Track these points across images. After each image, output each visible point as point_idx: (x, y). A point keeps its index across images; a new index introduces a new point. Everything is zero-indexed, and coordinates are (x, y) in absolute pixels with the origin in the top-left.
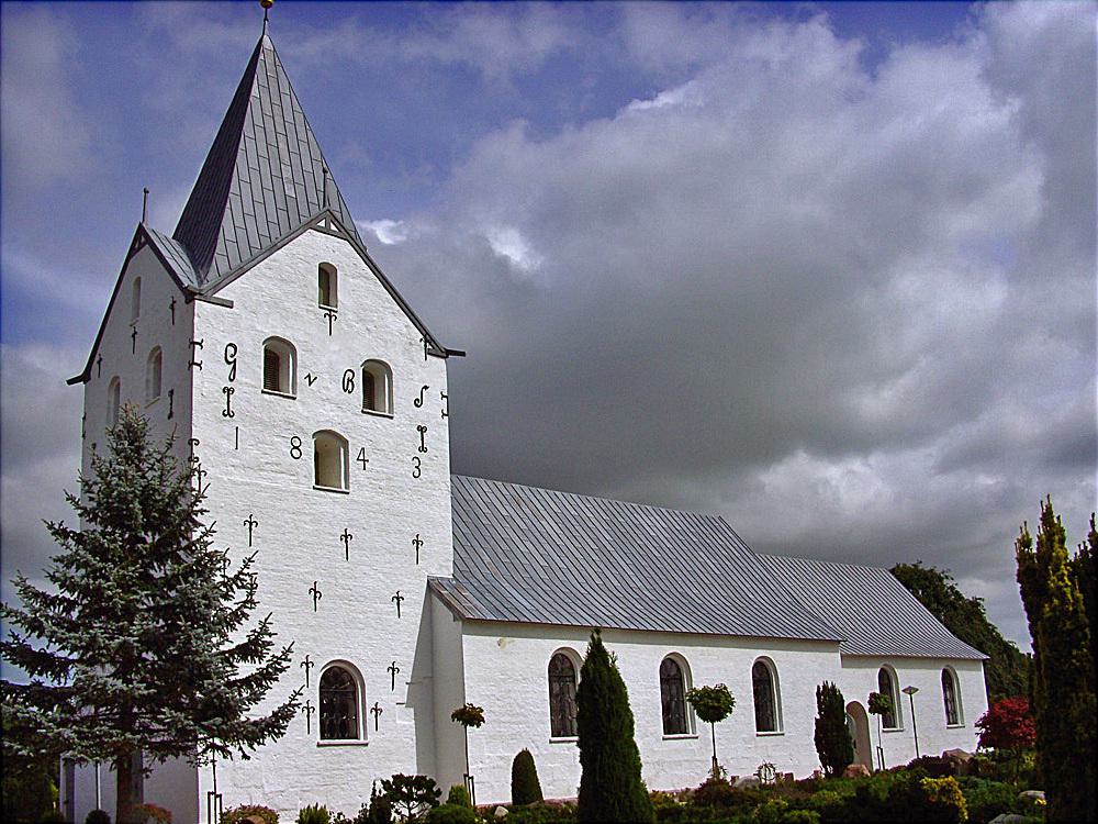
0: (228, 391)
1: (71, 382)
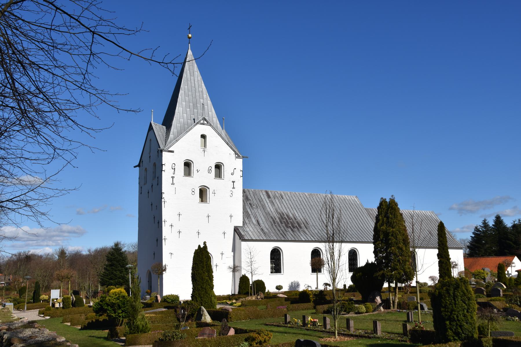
0: (173, 177)
1: (135, 167)
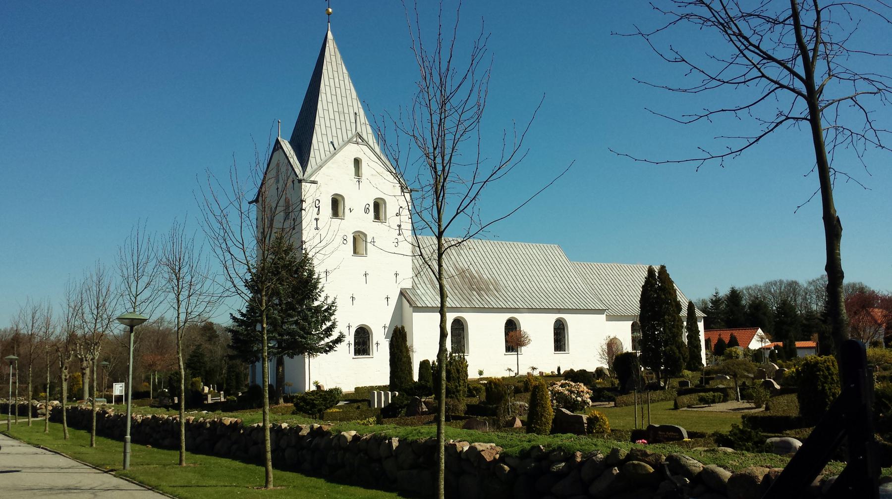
0: (317, 220)
